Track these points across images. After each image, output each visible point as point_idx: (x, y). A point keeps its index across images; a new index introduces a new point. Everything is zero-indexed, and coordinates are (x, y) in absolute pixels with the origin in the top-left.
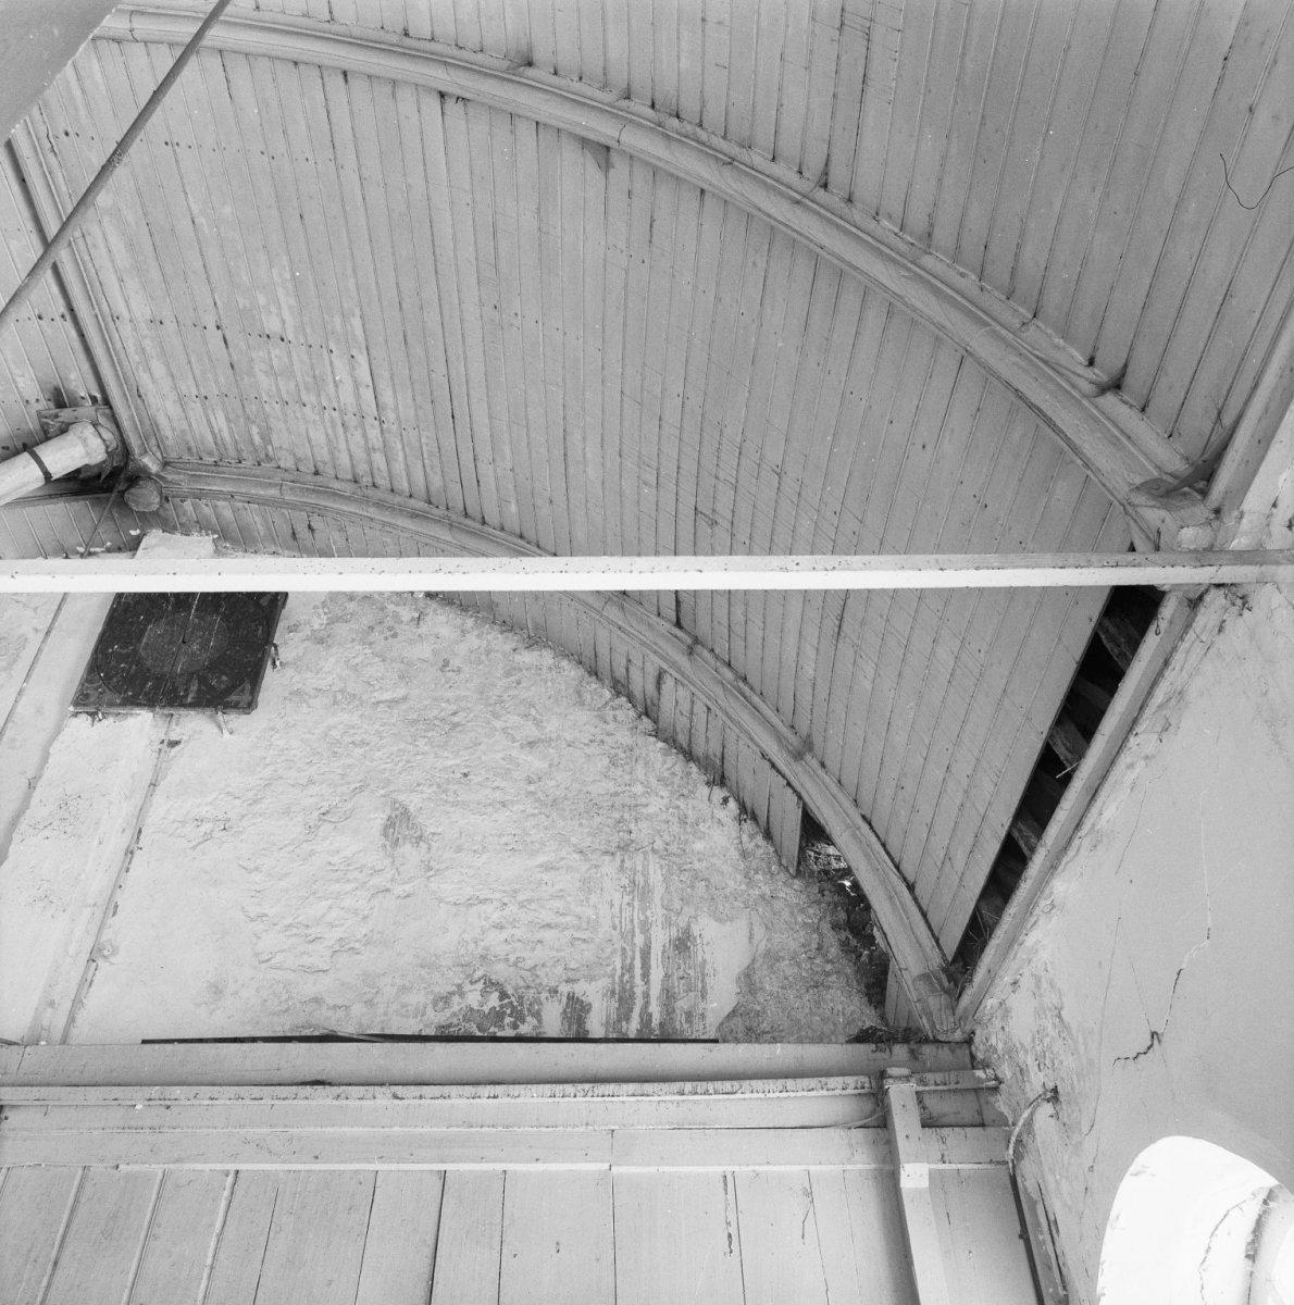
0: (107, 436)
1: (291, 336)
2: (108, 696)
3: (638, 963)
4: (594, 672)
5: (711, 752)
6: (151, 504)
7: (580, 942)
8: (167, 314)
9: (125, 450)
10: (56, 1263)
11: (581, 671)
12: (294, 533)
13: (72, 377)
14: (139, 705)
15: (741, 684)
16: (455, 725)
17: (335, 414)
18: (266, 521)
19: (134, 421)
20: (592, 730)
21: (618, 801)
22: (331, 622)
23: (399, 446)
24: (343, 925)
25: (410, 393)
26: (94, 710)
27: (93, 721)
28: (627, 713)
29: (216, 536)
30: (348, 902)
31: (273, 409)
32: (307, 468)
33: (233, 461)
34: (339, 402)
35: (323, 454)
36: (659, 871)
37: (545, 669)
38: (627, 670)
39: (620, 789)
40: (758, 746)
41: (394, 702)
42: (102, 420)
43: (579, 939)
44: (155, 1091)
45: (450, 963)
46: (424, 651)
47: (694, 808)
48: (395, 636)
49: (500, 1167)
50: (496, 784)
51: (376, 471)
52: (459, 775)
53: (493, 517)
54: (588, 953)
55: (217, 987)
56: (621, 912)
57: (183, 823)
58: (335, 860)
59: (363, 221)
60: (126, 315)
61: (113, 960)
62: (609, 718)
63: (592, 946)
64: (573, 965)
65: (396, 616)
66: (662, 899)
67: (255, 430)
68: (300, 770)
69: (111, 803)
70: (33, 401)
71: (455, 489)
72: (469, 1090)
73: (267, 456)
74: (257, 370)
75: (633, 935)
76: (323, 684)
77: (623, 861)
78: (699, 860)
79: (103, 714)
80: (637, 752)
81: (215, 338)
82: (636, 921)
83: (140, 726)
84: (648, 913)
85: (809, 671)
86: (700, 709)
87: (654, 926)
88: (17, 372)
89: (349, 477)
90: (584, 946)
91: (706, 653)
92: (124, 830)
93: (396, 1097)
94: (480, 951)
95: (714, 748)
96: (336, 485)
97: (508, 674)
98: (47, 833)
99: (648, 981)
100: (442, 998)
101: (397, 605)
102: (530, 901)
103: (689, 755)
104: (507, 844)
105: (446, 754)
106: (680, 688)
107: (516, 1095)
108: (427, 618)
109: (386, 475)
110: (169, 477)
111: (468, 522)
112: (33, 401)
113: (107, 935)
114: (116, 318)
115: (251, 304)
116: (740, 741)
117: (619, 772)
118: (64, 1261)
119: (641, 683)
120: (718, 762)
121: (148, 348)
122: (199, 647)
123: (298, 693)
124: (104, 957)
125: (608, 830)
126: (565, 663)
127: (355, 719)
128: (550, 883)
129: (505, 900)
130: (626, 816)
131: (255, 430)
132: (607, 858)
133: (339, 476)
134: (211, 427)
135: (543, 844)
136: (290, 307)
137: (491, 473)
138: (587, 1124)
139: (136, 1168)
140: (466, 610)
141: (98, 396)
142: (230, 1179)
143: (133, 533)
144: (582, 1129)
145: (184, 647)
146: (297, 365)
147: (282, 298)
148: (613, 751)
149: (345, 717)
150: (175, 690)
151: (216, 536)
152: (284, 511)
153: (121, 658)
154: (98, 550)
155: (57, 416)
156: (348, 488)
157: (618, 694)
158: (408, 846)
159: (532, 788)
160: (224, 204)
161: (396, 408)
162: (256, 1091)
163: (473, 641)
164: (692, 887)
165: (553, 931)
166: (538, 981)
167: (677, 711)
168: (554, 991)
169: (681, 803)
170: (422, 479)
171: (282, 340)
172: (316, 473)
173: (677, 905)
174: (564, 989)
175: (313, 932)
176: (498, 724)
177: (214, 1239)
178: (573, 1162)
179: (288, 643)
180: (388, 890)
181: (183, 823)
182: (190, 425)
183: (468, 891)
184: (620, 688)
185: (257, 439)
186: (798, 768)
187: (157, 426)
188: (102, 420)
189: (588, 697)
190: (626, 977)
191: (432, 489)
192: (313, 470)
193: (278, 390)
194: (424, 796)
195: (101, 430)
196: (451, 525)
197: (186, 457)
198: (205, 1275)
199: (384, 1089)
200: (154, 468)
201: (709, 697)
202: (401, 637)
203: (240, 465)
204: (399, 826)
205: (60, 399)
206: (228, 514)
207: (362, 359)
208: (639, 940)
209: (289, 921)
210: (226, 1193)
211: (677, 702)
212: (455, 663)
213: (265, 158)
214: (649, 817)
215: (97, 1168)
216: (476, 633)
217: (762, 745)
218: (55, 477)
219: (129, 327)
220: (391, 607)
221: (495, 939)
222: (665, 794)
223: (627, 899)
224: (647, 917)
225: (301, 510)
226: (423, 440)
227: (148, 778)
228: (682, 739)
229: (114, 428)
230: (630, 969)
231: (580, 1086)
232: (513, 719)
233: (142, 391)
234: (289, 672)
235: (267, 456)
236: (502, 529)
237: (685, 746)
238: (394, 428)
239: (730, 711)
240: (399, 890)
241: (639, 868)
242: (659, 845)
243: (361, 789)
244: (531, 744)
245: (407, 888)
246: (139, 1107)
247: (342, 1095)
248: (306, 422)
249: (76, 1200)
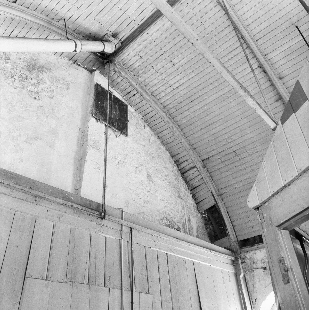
3: (185, 222)
85: (237, 186)
96: (147, 91)
136: (184, 62)
143: (94, 68)
154: (82, 66)
156: (150, 94)
178: (181, 255)
185: (141, 72)
186: (218, 197)
203: (130, 72)
207: (185, 79)
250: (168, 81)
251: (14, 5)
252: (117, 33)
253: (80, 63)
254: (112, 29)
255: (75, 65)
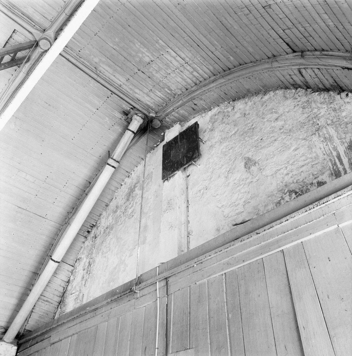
0: (140, 115)
1: (153, 59)
2: (168, 173)
3: (337, 161)
4: (287, 88)
5: (331, 83)
6: (158, 124)
7: (315, 165)
8: (128, 76)
9: (146, 116)
10: (190, 313)
11: (283, 90)
12: (193, 109)
13: (124, 106)
14: (175, 171)
15: (323, 53)
16: (253, 128)
17: (177, 70)
18: (185, 110)
19: (142, 107)
20: (294, 103)
21: (310, 118)
22: (213, 124)
23: (196, 66)
24: (243, 197)
25: (185, 49)
26: (167, 178)
27: (168, 181)
28: (301, 91)
29: (179, 123)
30: (242, 191)
31: (165, 81)
32: (184, 90)
33: (169, 101)
34: (175, 66)
35: (184, 83)
36: (333, 130)
37: (272, 97)
38: (292, 79)
39: (309, 114)
40: (339, 66)
41: (235, 134)
42: (137, 112)
43: (314, 165)
44: (196, 260)
45: (276, 192)
46: (238, 115)
47: (337, 104)
48: (229, 116)
49: (299, 241)
50: (271, 136)
51: (197, 77)
52: (260, 140)
53: (231, 66)
54: (319, 167)
55: (218, 229)
56: (325, 149)
57: (197, 193)
58: (235, 182)
59: (139, 13)
60: (122, 83)
61: (192, 234)
62: (297, 97)
63: (319, 164)
64: (315, 173)
65: (228, 112)
66: (337, 137)
67: (166, 90)
68: (219, 164)
69: (178, 197)
70: (121, 118)
71: (216, 66)
72: (279, 221)
73: (174, 94)
74: (154, 74)
75: (332, 153)
76: (216, 140)
77: (319, 134)
78: (346, 118)
79: (169, 178)
80: (310, 100)
81: (140, 73)
82: (331, 149)
83: (179, 175)
84: (334, 144)
85: (331, 24)
86: (317, 71)
87: (338, 147)
88: (114, 113)
89: (194, 84)
90: (317, 165)
91: (308, 53)
92: (185, 202)
93: (257, 234)
94: (284, 184)
95: (331, 81)
96: (193, 89)
97: (262, 105)
98: (167, 212)
99: (343, 164)
100: (278, 203)
101: (227, 109)
102: (294, 162)
103: (327, 90)
104: (280, 150)
105: (254, 137)
106: (307, 70)
107: (294, 216)
108: (235, 107)
109: (200, 77)
110: (159, 115)
111: (226, 72)
112: (121, 118)
113: (189, 229)
114: (120, 86)
115: (139, 58)
116: (334, 70)
117: (307, 110)
118: (192, 311)
119: (298, 79)
120: (336, 84)
121: (131, 88)
122: (182, 149)
123: (211, 146)
124: (191, 234)
125: (311, 128)
126: (277, 92)
127: (227, 143)
128: (298, 154)
129: (286, 166)
130: (315, 120)
131: (166, 90)
132: (313, 136)
133: (192, 86)
134: (158, 97)
135: (291, 144)
137: (219, 53)
138: (323, 215)
139: (200, 282)
140: (245, 97)
141: (132, 107)
142: (224, 276)
144: (322, 217)
145: (180, 152)
146: (160, 65)
147: (143, 51)
148: (303, 105)
149: (225, 144)
150: (181, 163)
151: (179, 123)
152: (187, 104)
153: (168, 163)
154: (159, 143)
155: (128, 118)
157: (297, 88)
158: (253, 167)
159: (282, 131)
160: (115, 39)
161: (187, 56)
162: (220, 249)
163: (250, 103)
164: (347, 128)
165: (305, 166)
166: (306, 183)
167: (313, 78)
168: (312, 184)
169: (332, 106)
170: (207, 70)
171: (152, 61)
172: (187, 89)
173: (343, 136)
174: (315, 181)
175: (237, 203)
176: (265, 120)
177: (225, 294)
179: (204, 136)
180: (252, 182)
181: (197, 193)
182: (154, 100)
183: (274, 169)
184: (296, 86)
187: (148, 105)
188: (137, 112)
189: (288, 96)
190: (335, 167)
191: (212, 71)
192: (185, 89)
193: (162, 75)
194: (253, 151)
195: (138, 114)
196: (223, 77)
197: (160, 108)
198: (226, 305)
199: (253, 233)
200: (154, 115)
201: (316, 65)
202: (231, 116)
203: (171, 101)
204: (249, 163)
205: (126, 113)
206: (176, 115)
207: (170, 50)
208: (335, 154)
209: (230, 203)
210: (224, 280)
211: (310, 75)
212: (247, 113)
213: (112, 19)
214: (323, 116)
215: (192, 285)
216: (249, 101)
217: (340, 65)
218: (135, 132)
219: (124, 86)
220: (226, 110)
221: (287, 179)
222: (325, 106)
223: (325, 144)
224: (334, 145)
225: (189, 102)
226: (199, 59)
227: (186, 187)
228: (321, 86)
229: (140, 112)
230: (335, 164)
231: (314, 204)
232: (269, 116)
233: (139, 99)
234: (207, 142)
235: (174, 94)
236: (235, 67)
237: (323, 88)
238: (191, 62)
239: (324, 63)
240: (255, 180)
241: (325, 132)
242: (329, 122)
243: (235, 160)
244: (277, 119)
245: (257, 178)
246: (195, 266)
247: (243, 240)
248: (174, 78)
249: (190, 296)
250: (175, 68)
251: (92, 184)
252: (124, 112)
253: (154, 145)
254: (119, 115)
255: (156, 149)
